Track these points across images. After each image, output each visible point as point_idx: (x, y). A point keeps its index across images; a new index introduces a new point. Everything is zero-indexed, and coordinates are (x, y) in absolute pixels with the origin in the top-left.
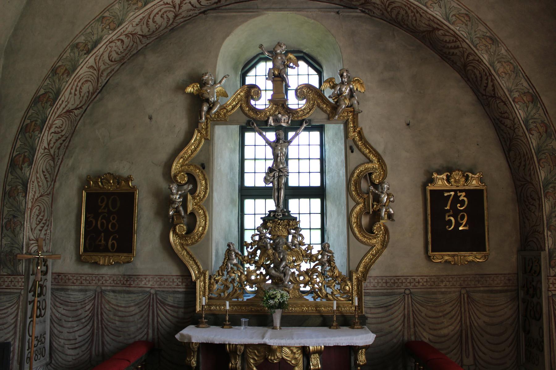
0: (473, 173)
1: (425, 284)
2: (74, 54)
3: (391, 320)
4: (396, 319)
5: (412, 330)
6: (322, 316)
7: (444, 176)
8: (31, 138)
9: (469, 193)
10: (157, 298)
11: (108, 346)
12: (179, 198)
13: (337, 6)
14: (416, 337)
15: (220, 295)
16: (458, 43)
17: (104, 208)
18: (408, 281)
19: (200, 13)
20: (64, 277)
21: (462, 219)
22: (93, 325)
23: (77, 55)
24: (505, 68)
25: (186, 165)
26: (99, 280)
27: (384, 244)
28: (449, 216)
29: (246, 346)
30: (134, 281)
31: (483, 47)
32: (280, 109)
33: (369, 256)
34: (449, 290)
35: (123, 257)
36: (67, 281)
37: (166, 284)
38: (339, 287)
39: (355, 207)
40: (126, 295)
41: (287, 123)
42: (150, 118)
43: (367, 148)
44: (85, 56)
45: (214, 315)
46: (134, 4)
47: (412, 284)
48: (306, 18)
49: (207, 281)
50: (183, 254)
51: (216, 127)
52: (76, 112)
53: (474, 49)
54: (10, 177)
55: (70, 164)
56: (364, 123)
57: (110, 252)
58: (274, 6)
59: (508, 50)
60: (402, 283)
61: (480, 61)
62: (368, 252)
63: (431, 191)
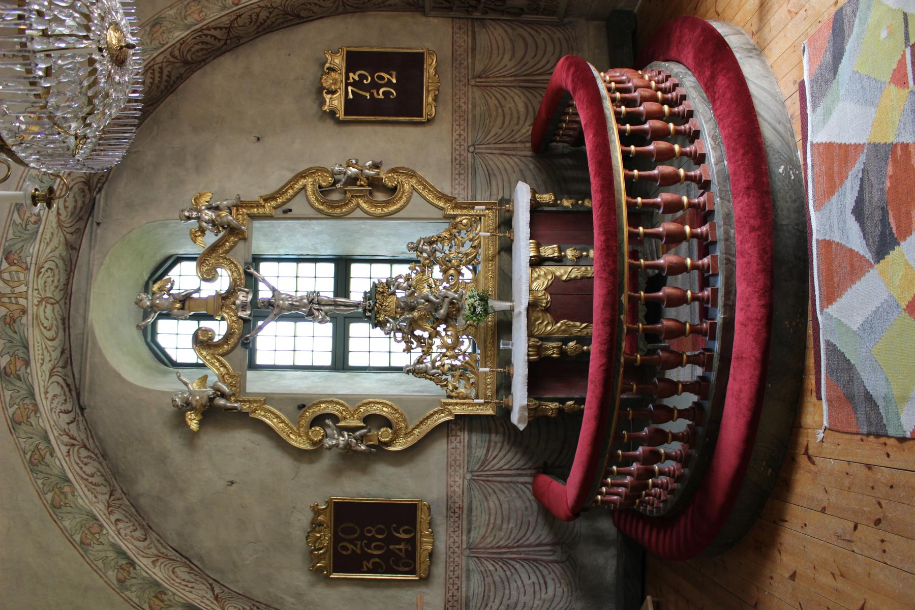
0: (326, 62)
1: (462, 127)
2: (133, 585)
3: (506, 170)
4: (506, 164)
5: (519, 145)
6: (499, 253)
7: (327, 97)
9: (350, 68)
10: (477, 471)
11: (541, 538)
12: (343, 436)
13: (88, 225)
14: (527, 142)
15: (473, 383)
16: (156, 67)
17: (355, 545)
18: (458, 147)
19: (83, 415)
20: (450, 604)
21: (382, 78)
22: (514, 559)
23: (134, 581)
24: (193, 12)
25: (298, 429)
26: (454, 553)
27: (411, 174)
28: (378, 94)
29: (530, 335)
30: (455, 503)
31: (165, 36)
32: (228, 302)
33: (425, 193)
34: (470, 99)
35: (422, 517)
36: (455, 598)
37: (458, 458)
38: (463, 232)
39: (362, 209)
40: (474, 514)
41: (247, 293)
42: (232, 483)
43: (286, 191)
44: (138, 568)
45: (498, 391)
46: (66, 498)
47: (462, 143)
48: (103, 267)
49: (454, 401)
50: (418, 434)
51: (248, 391)
52: (217, 590)
53: (166, 47)
55: (293, 600)
56: (254, 194)
57: (415, 535)
58: (81, 311)
59: (171, 7)
60: (460, 155)
61: (183, 42)
62: (420, 194)
63: (346, 114)
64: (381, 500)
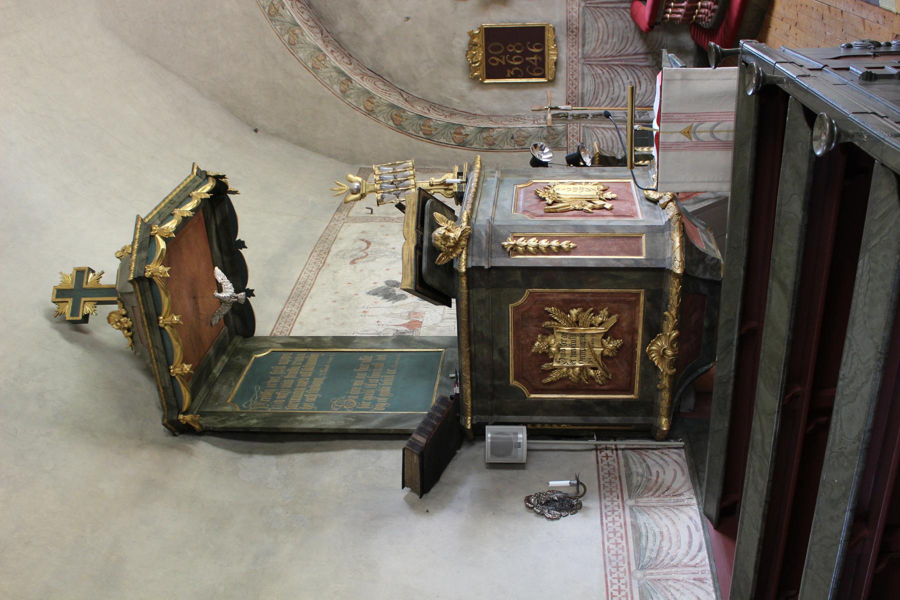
8: (436, 129)
17: (501, 59)
22: (617, 65)
23: (352, 91)
35: (549, 36)
40: (587, 32)
54: (475, 146)
55: (458, 101)
64: (518, 24)
